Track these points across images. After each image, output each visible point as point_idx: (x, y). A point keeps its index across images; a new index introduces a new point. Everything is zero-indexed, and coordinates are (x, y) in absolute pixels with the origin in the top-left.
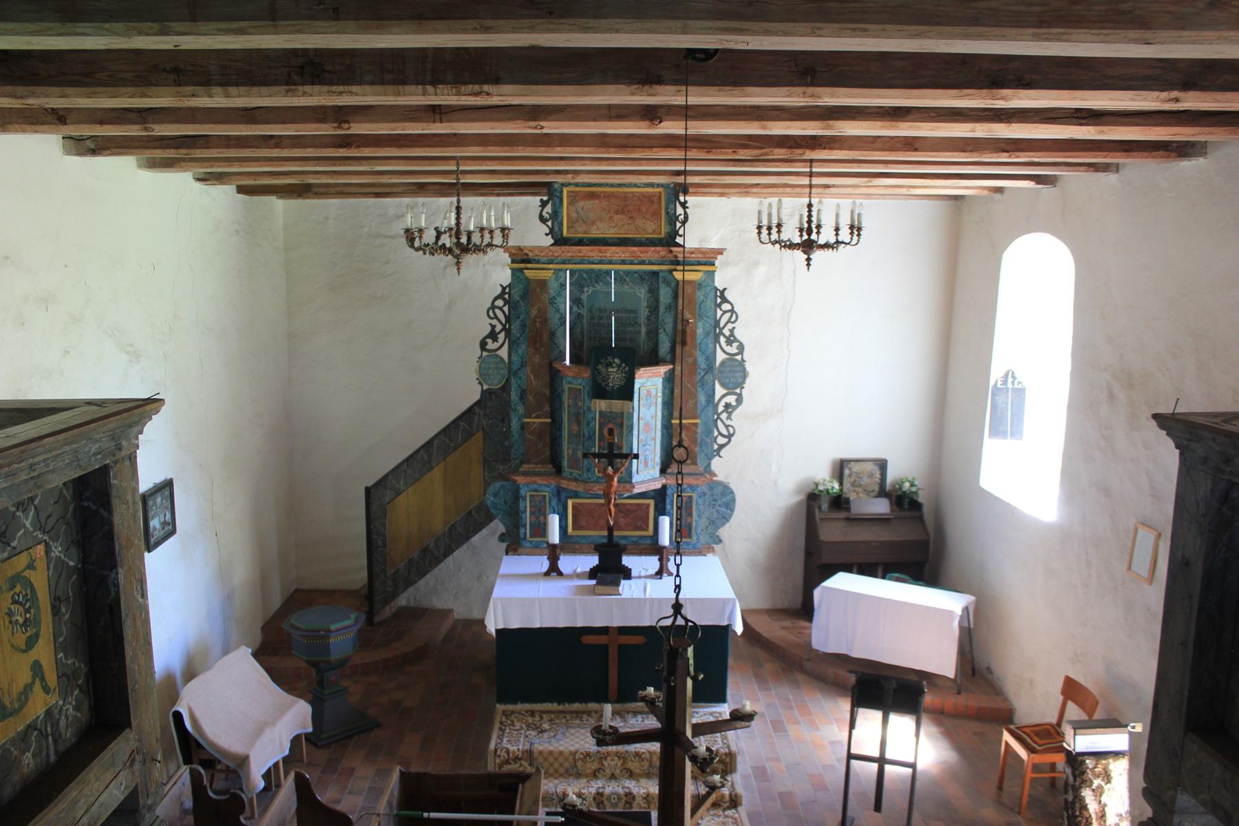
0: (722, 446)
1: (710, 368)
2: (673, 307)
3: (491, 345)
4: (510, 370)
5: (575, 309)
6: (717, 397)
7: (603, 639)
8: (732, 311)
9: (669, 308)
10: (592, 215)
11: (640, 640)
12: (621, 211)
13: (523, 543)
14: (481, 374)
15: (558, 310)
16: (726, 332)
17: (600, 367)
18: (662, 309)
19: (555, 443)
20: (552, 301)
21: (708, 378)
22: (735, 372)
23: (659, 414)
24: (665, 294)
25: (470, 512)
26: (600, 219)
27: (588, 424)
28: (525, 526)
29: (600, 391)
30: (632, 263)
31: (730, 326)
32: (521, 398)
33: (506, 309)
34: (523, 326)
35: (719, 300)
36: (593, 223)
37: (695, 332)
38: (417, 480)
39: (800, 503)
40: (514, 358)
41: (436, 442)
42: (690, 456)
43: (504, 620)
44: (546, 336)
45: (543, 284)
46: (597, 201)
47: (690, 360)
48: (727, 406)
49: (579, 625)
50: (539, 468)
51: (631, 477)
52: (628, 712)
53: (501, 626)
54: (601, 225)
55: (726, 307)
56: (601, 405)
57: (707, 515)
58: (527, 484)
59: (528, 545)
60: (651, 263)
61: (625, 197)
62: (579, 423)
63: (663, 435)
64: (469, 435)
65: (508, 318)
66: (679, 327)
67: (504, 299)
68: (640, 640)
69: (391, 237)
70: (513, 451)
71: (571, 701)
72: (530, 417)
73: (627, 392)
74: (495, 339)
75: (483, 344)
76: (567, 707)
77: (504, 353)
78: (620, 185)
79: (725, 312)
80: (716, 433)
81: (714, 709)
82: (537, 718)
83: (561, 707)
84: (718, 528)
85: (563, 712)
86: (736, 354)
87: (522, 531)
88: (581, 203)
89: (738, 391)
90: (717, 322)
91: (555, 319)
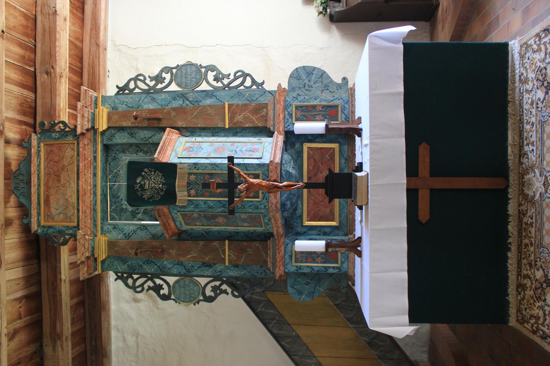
0: (254, 82)
1: (182, 96)
2: (130, 130)
3: (165, 291)
4: (185, 275)
5: (140, 216)
6: (209, 88)
7: (424, 198)
8: (136, 79)
9: (132, 135)
10: (61, 201)
11: (424, 151)
12: (58, 177)
13: (343, 270)
14: (190, 301)
15: (135, 232)
16: (152, 84)
17: (145, 196)
18: (133, 141)
19: (250, 237)
20: (127, 236)
21: (191, 96)
22: (186, 73)
23: (206, 139)
24: (121, 138)
25: (336, 305)
26: (64, 195)
27: (211, 207)
28: (325, 267)
29: (169, 197)
30: (95, 168)
31: (148, 81)
32: (210, 266)
33: (135, 276)
34: (148, 262)
35: (127, 92)
36: (67, 200)
37: (149, 110)
38: (308, 349)
39: (338, 28)
40: (175, 271)
41: (275, 331)
42: (260, 108)
43: (398, 314)
44: (155, 243)
45: (111, 245)
46: (51, 198)
47: (173, 114)
48: (216, 79)
49: (405, 225)
50: (270, 252)
51: (263, 165)
52: (521, 163)
53: (406, 318)
54: (69, 194)
55: (132, 85)
56: (182, 195)
57: (318, 93)
58: (285, 265)
59: (345, 265)
60: (95, 152)
61: (48, 174)
62: (214, 217)
63: (242, 136)
64: (269, 304)
65: (143, 275)
66: (145, 124)
67: (127, 278)
68: (424, 151)
69: (138, 347)
70: (259, 276)
71: (506, 234)
72: (224, 259)
73: (170, 170)
74: (160, 287)
75: (165, 298)
76: (513, 240)
77: (171, 280)
78: (39, 179)
79: (136, 86)
80: (242, 87)
81: (517, 56)
82: (527, 282)
83: (514, 248)
84: (332, 81)
85: (519, 246)
86: (172, 74)
87: (331, 271)
88: (53, 210)
89: (203, 70)
90: (145, 92)
91: (142, 235)
